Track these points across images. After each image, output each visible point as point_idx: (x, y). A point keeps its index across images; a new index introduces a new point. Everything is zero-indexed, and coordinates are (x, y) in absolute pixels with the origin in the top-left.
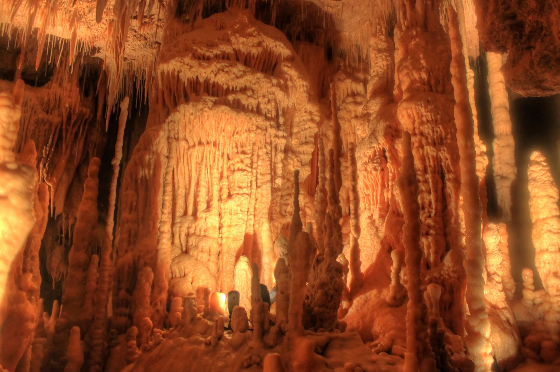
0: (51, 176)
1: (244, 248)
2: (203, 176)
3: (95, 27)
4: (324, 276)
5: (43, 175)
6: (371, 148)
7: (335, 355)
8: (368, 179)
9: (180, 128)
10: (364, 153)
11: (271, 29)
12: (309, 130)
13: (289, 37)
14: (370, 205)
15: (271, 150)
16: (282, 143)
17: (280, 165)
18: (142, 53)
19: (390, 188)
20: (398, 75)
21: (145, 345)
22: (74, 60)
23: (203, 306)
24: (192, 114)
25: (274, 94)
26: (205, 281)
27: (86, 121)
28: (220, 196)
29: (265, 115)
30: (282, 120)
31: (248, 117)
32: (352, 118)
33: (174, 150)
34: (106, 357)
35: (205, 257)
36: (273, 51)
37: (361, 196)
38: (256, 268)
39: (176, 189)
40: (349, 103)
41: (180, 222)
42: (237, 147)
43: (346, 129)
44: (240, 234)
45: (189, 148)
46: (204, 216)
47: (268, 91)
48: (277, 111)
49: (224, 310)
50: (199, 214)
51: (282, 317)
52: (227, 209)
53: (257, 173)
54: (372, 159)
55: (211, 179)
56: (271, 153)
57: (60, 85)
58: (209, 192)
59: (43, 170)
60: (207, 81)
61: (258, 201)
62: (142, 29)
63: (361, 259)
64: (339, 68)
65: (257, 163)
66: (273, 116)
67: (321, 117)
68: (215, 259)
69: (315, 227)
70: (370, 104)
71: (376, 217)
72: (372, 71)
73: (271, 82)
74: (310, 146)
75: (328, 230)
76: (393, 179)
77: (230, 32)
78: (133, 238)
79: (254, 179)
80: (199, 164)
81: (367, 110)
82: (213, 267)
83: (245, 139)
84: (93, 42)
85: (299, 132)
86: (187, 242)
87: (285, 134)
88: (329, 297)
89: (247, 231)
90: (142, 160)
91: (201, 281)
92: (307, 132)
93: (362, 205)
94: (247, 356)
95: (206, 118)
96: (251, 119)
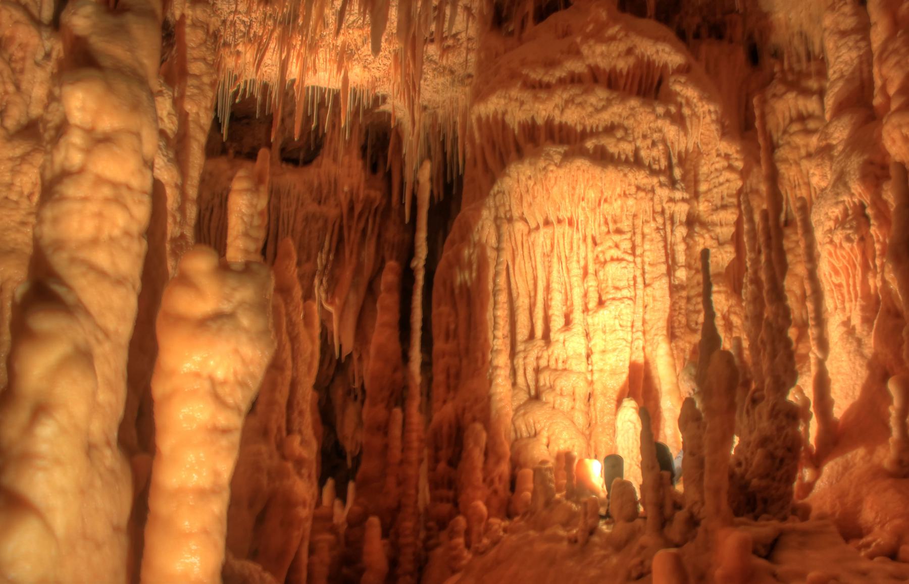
0: (333, 297)
1: (630, 387)
2: (555, 274)
3: (374, 66)
4: (765, 425)
5: (319, 295)
6: (837, 203)
7: (790, 560)
8: (837, 257)
9: (513, 201)
10: (827, 214)
11: (649, 24)
12: (727, 185)
13: (682, 35)
14: (843, 302)
15: (664, 224)
16: (681, 210)
17: (681, 248)
18: (449, 95)
19: (879, 270)
20: (880, 70)
21: (477, 545)
22: (349, 119)
23: (565, 481)
24: (530, 178)
25: (660, 131)
26: (569, 442)
27: (376, 209)
28: (586, 305)
29: (650, 166)
30: (680, 172)
31: (621, 174)
32: (801, 158)
33: (506, 237)
34: (421, 565)
35: (566, 403)
36: (654, 61)
37: (826, 287)
38: (650, 417)
39: (514, 299)
40: (795, 133)
41: (525, 351)
42: (606, 223)
43: (791, 178)
44: (621, 363)
45: (530, 232)
46: (561, 337)
47: (650, 128)
48: (669, 159)
49: (600, 486)
50: (553, 336)
51: (693, 496)
52: (598, 324)
53: (643, 262)
54: (841, 223)
55: (569, 277)
56: (664, 229)
57: (335, 160)
58: (567, 299)
59: (319, 288)
60: (549, 123)
61: (648, 308)
62: (445, 58)
63: (833, 396)
64: (772, 77)
65: (642, 246)
66: (663, 168)
67: (745, 160)
68: (582, 406)
69: (745, 344)
70: (831, 129)
71: (856, 321)
72: (831, 72)
73: (654, 111)
74: (730, 211)
75: (768, 348)
76: (883, 254)
77: (578, 40)
78: (455, 380)
79: (638, 273)
80: (548, 256)
81: (826, 139)
82: (580, 419)
83: (619, 210)
84: (374, 88)
85: (710, 190)
86: (537, 381)
87: (686, 196)
88: (778, 461)
89: (633, 358)
90: (458, 258)
91: (562, 441)
92: (724, 189)
93: (829, 303)
94: (636, 561)
95: (553, 181)
96: (625, 175)
